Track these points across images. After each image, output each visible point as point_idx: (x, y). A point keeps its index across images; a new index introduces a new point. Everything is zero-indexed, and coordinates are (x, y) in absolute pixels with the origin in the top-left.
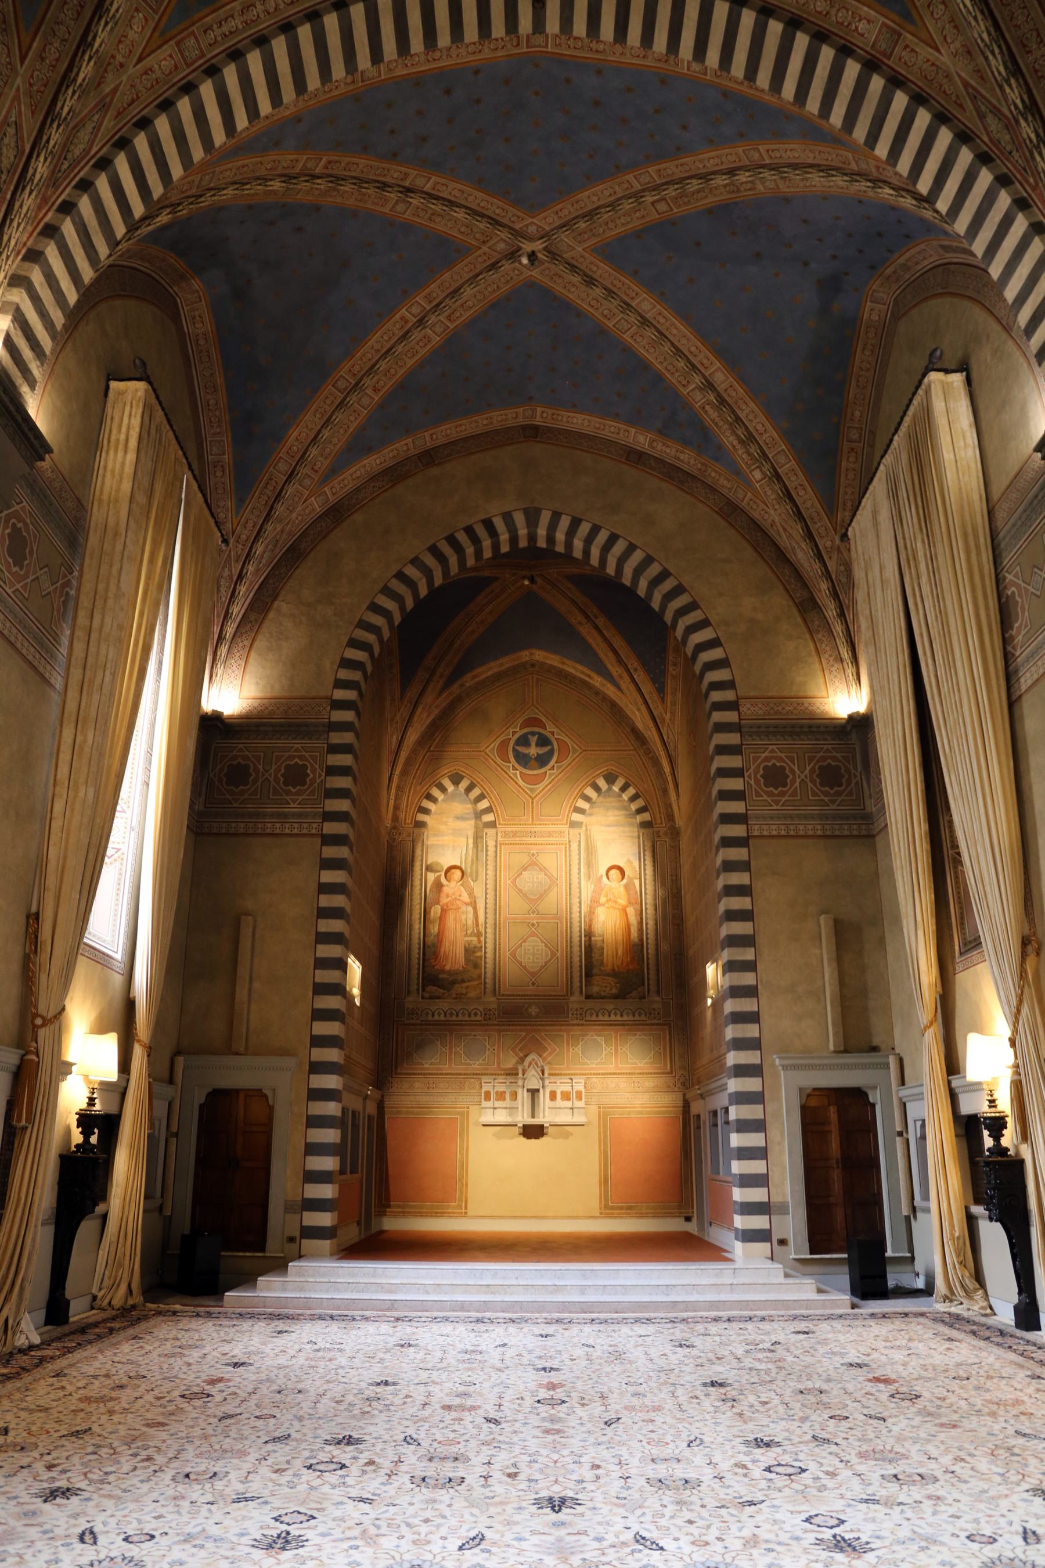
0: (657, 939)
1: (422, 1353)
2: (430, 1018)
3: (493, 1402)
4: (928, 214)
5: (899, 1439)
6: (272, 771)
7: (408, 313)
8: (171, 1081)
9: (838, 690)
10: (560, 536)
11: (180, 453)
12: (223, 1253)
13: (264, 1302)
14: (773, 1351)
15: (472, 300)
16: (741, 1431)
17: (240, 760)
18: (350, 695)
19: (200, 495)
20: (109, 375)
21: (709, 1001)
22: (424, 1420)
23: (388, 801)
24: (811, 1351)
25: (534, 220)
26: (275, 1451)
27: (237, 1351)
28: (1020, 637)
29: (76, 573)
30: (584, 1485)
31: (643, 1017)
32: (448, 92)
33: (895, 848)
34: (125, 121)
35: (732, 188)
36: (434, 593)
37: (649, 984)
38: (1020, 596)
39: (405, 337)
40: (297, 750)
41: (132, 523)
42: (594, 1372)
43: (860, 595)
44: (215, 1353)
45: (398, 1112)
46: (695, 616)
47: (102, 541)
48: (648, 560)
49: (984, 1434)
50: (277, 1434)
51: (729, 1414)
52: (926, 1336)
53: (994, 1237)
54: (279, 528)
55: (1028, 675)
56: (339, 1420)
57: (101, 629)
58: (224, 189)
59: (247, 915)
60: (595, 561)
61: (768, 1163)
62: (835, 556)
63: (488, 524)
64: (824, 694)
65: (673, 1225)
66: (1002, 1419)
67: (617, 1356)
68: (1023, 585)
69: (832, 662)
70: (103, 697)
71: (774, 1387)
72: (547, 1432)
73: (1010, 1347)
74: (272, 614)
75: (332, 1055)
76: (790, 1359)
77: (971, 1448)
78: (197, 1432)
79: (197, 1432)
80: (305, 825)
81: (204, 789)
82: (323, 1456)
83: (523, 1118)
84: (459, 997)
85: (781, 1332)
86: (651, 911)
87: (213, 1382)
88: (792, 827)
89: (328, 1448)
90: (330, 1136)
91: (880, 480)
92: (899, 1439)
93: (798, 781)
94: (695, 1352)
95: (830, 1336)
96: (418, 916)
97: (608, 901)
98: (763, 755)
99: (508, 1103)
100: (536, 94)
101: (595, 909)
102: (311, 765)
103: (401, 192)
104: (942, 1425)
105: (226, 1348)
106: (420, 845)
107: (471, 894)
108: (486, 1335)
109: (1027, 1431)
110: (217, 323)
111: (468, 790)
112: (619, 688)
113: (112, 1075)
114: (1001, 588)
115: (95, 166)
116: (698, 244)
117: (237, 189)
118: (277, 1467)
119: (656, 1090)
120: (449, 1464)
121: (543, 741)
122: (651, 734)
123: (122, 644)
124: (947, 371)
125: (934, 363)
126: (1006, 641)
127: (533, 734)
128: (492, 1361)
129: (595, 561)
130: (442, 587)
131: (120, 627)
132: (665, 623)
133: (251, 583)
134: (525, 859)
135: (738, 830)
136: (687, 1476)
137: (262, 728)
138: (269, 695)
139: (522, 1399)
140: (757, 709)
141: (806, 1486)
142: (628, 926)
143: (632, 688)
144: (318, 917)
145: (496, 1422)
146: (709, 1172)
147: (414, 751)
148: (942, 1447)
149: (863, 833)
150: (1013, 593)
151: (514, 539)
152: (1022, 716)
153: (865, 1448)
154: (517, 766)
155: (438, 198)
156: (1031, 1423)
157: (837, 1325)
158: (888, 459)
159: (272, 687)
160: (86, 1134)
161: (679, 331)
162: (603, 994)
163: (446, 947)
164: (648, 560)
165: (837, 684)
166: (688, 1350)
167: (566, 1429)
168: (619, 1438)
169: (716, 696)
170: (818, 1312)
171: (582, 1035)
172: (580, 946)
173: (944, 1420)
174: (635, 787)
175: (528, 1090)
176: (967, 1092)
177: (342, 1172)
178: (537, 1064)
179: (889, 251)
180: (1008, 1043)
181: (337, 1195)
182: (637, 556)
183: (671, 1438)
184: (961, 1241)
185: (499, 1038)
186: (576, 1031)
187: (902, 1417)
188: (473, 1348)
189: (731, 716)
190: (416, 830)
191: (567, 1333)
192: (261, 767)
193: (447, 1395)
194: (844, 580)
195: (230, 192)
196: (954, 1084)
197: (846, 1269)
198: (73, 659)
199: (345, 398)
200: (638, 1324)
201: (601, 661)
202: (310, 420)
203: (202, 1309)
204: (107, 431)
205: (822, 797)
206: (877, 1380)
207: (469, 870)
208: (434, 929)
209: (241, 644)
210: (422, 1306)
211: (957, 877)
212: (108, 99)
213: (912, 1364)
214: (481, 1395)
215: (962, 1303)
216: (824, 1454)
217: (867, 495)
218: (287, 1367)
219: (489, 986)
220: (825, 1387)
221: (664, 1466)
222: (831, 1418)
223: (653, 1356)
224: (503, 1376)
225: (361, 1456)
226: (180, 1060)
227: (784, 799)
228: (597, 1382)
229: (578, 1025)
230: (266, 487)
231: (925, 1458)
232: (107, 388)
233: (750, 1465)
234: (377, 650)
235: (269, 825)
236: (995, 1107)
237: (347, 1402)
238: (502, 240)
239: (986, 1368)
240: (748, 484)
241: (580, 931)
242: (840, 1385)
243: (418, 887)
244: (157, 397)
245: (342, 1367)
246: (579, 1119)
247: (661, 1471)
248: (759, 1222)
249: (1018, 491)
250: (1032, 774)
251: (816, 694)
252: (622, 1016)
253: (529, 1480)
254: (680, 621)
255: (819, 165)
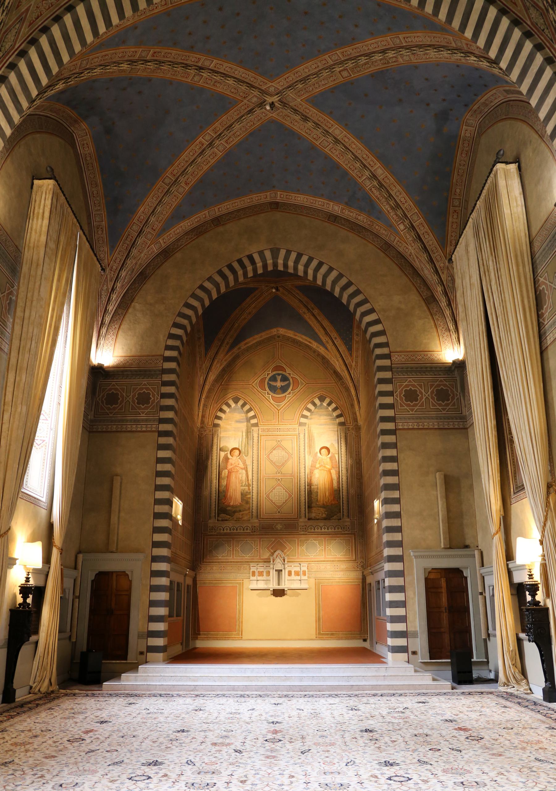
0: (347, 487)
1: (207, 714)
2: (222, 531)
3: (240, 741)
4: (496, 71)
5: (467, 762)
6: (131, 396)
7: (203, 139)
8: (75, 568)
9: (447, 347)
10: (291, 264)
11: (75, 220)
12: (103, 662)
13: (125, 687)
14: (403, 713)
15: (240, 131)
16: (378, 757)
17: (113, 391)
18: (174, 354)
19: (87, 244)
20: (33, 177)
21: (376, 521)
22: (200, 751)
23: (198, 413)
24: (425, 713)
25: (272, 84)
26: (113, 770)
27: (104, 715)
28: (547, 314)
29: (16, 287)
30: (283, 787)
31: (340, 530)
32: (221, 9)
33: (477, 435)
34: (34, 29)
35: (384, 61)
36: (221, 297)
37: (343, 512)
38: (547, 290)
39: (201, 153)
40: (145, 385)
41: (47, 259)
42: (300, 724)
43: (459, 294)
44: (92, 716)
45: (204, 583)
46: (367, 307)
47: (30, 269)
48: (340, 276)
49: (517, 760)
50: (116, 761)
51: (372, 747)
52: (491, 705)
53: (532, 651)
54: (134, 262)
55: (551, 335)
56: (152, 752)
57: (29, 319)
58: (95, 69)
59: (117, 475)
60: (310, 277)
61: (407, 610)
62: (445, 272)
63: (251, 258)
64: (439, 349)
65: (357, 643)
66: (529, 751)
67: (315, 715)
68: (549, 284)
69: (444, 332)
70: (31, 356)
71: (400, 732)
72: (268, 757)
73: (539, 711)
74: (130, 310)
75: (164, 552)
76: (412, 717)
77: (508, 767)
78: (72, 760)
79: (72, 760)
80: (149, 426)
81: (94, 407)
82: (139, 772)
83: (274, 585)
84: (238, 520)
85: (410, 702)
86: (344, 471)
87: (87, 732)
88: (421, 424)
89: (143, 767)
90: (163, 596)
91: (469, 227)
92: (467, 762)
93: (424, 398)
94: (359, 713)
95: (437, 704)
96: (215, 476)
97: (320, 466)
98: (405, 384)
99: (265, 577)
100: (271, 9)
101: (313, 471)
102: (152, 393)
103: (196, 69)
104: (493, 754)
105: (99, 713)
106: (216, 437)
107: (244, 463)
108: (244, 704)
109: (542, 758)
110: (97, 149)
111: (243, 406)
112: (327, 349)
113: (38, 563)
114: (537, 286)
115: (17, 55)
116: (366, 95)
117: (102, 69)
118: (112, 779)
119: (347, 570)
120: (209, 776)
121: (285, 379)
122: (345, 374)
123: (42, 326)
124: (507, 163)
125: (499, 159)
126: (539, 316)
127: (279, 374)
128: (244, 718)
129: (310, 277)
130: (225, 294)
131: (41, 317)
132: (350, 311)
133: (119, 293)
134: (274, 443)
135: (390, 426)
136: (342, 782)
137: (125, 373)
138: (129, 355)
139: (257, 739)
140: (401, 358)
141: (410, 788)
142: (332, 480)
143: (334, 347)
144: (156, 476)
145: (240, 752)
146: (376, 615)
147: (213, 385)
148: (492, 767)
149: (461, 426)
150: (543, 288)
151: (265, 266)
152: (548, 359)
153: (447, 767)
154: (270, 392)
155: (217, 72)
156: (545, 753)
157: (442, 698)
158: (474, 215)
159: (131, 350)
160: (25, 597)
161: (357, 146)
162: (318, 517)
163: (231, 492)
164: (340, 276)
165: (447, 343)
166: (356, 712)
167: (279, 756)
168: (307, 761)
169: (378, 351)
170: (432, 691)
171: (306, 540)
172: (305, 491)
173: (495, 752)
174: (336, 403)
175: (276, 570)
176: (517, 570)
177: (170, 615)
178: (281, 556)
179: (475, 95)
180: (539, 543)
181: (167, 629)
182: (334, 274)
183: (337, 761)
184: (514, 652)
185: (260, 541)
186: (303, 538)
187: (471, 749)
188: (235, 711)
189: (387, 362)
190: (214, 429)
191: (289, 703)
192: (125, 394)
193: (216, 737)
194: (450, 285)
195: (98, 71)
196: (510, 566)
197: (450, 668)
198: (14, 334)
199: (169, 189)
200: (330, 697)
201: (316, 334)
202: (150, 201)
203: (90, 692)
204: (33, 207)
205: (438, 407)
206: (460, 729)
207: (243, 450)
208: (224, 483)
209: (114, 327)
210: (212, 688)
211: (512, 451)
212: (24, 16)
213: (481, 720)
214: (234, 737)
215: (514, 687)
216: (423, 770)
217: (462, 236)
218: (130, 723)
219: (255, 514)
220: (429, 732)
221: (331, 776)
222: (430, 750)
223: (335, 715)
224: (249, 726)
225: (160, 772)
226: (81, 556)
227: (416, 408)
228: (301, 730)
229: (304, 534)
230: (126, 239)
231: (480, 773)
232: (33, 184)
233: (379, 776)
234: (189, 329)
235: (129, 426)
236: (532, 578)
237: (159, 742)
238: (255, 96)
239: (523, 723)
240: (397, 233)
241: (305, 483)
242: (438, 732)
243: (216, 460)
244: (61, 189)
245: (161, 723)
246: (304, 586)
247: (328, 779)
248: (401, 642)
249: (546, 230)
250: (554, 391)
251: (435, 349)
252: (328, 529)
253: (252, 784)
254: (358, 310)
255: (434, 45)
